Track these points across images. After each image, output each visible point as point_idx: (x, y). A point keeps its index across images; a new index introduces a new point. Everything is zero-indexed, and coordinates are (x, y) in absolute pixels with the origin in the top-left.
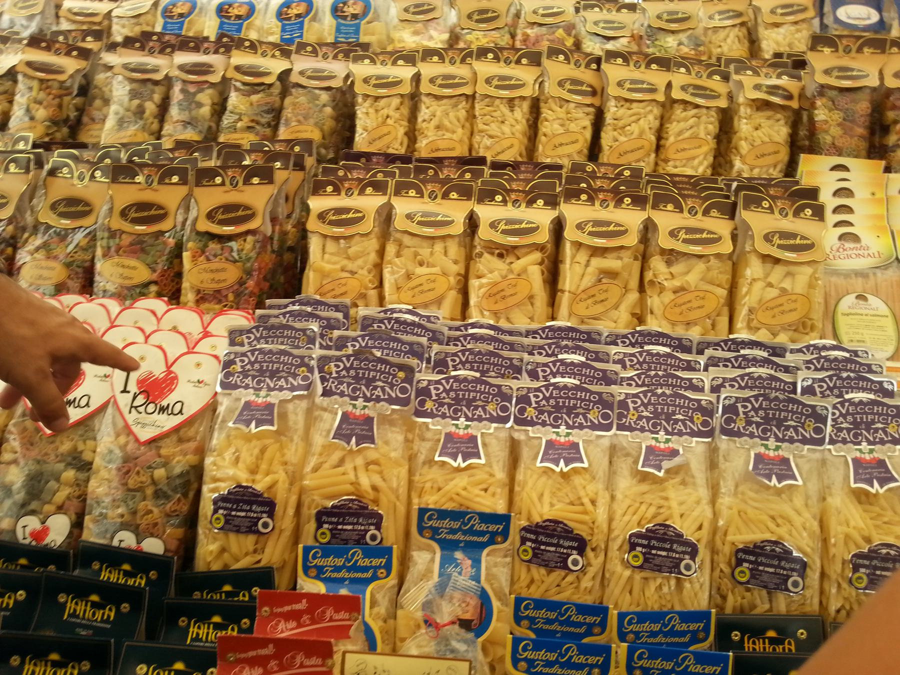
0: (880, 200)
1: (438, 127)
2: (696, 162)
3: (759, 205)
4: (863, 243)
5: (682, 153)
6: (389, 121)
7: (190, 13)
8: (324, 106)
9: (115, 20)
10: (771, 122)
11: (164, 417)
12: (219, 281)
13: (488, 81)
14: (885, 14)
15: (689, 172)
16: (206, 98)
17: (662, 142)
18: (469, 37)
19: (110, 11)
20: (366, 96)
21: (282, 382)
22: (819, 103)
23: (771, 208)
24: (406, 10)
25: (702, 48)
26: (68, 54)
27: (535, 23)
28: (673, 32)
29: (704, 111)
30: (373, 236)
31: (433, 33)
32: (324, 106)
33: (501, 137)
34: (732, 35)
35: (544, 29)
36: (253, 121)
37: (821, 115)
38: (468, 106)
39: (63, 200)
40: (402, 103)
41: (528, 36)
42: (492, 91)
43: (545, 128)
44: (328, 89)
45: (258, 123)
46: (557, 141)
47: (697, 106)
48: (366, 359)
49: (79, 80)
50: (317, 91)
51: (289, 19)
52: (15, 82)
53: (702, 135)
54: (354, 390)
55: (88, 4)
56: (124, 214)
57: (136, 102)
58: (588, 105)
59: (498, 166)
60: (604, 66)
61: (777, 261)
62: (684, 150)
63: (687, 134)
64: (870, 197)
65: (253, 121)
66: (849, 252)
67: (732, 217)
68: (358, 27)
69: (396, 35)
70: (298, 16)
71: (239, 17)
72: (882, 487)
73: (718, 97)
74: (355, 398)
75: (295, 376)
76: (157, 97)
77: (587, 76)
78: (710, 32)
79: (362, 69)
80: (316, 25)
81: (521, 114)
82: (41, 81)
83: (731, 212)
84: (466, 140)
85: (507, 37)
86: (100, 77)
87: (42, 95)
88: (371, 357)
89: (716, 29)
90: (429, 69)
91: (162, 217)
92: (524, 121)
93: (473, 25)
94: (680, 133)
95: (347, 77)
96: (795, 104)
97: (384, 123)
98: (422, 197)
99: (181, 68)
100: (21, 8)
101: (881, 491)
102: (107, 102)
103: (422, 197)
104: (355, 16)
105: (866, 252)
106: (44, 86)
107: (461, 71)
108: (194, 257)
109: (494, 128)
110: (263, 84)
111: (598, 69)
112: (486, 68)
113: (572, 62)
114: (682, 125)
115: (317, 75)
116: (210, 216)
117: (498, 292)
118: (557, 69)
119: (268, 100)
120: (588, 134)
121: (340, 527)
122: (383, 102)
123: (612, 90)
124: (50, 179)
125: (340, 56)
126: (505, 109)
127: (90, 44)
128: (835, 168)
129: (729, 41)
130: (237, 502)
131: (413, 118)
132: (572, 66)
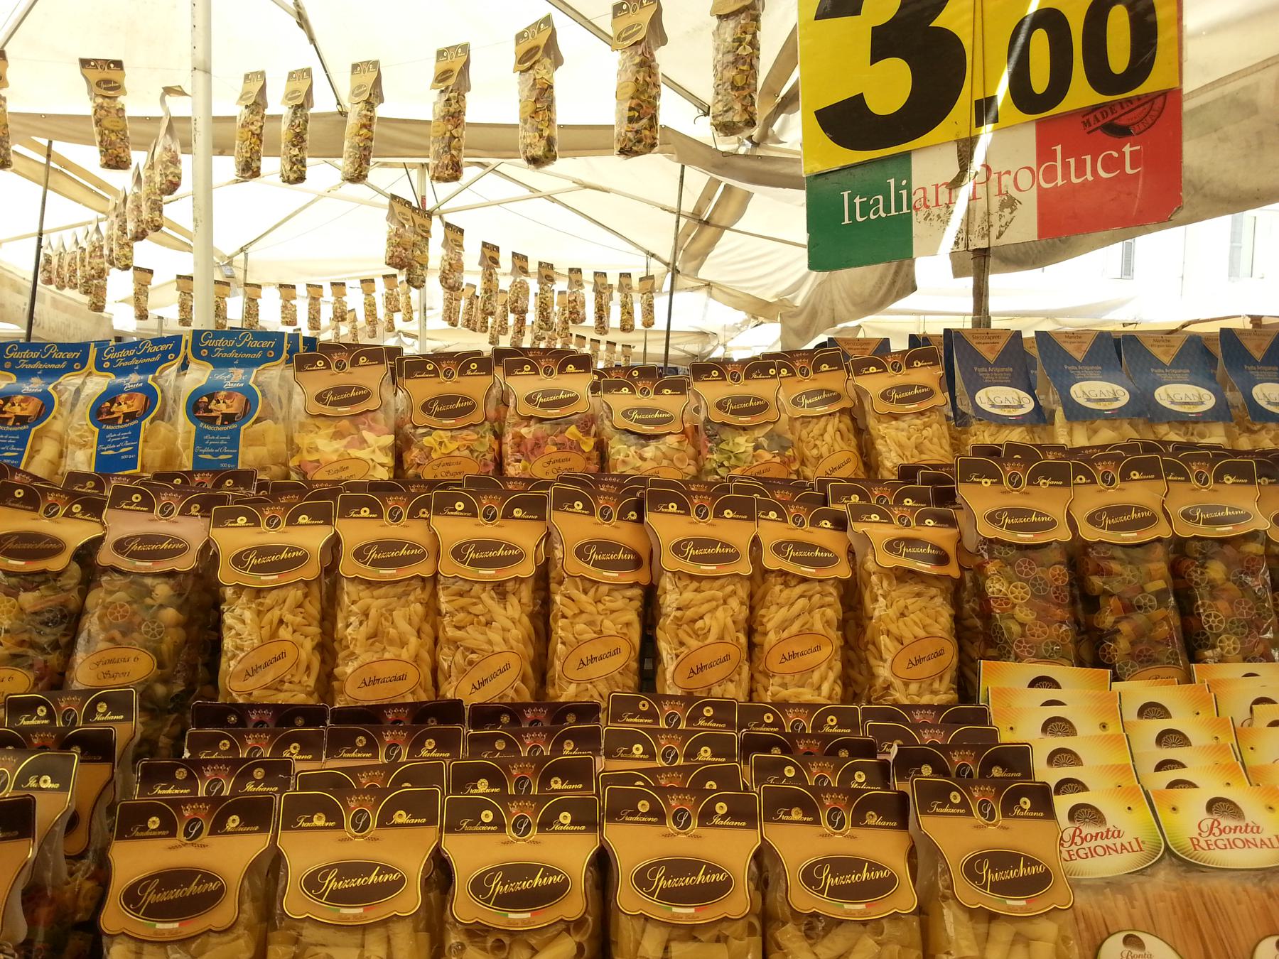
0: (1115, 739)
1: (374, 636)
2: (816, 676)
3: (946, 801)
4: (1110, 823)
5: (792, 662)
6: (284, 633)
8: (161, 606)
10: (921, 602)
13: (458, 553)
14: (1041, 398)
15: (808, 696)
17: (757, 639)
18: (427, 441)
20: (239, 589)
22: (991, 568)
23: (964, 804)
24: (320, 398)
25: (789, 453)
27: (531, 417)
28: (744, 429)
29: (817, 587)
30: (240, 930)
31: (367, 435)
32: (161, 606)
33: (488, 663)
34: (830, 428)
35: (546, 426)
36: (22, 643)
37: (995, 587)
38: (425, 596)
40: (306, 596)
41: (522, 437)
43: (561, 629)
44: (171, 574)
45: (33, 645)
46: (586, 652)
47: (804, 580)
50: (149, 581)
51: (114, 421)
53: (818, 626)
58: (631, 586)
59: (485, 715)
60: (650, 517)
61: (992, 917)
62: (793, 656)
63: (795, 628)
64: (1100, 732)
65: (22, 643)
66: (1093, 844)
67: (904, 825)
68: (235, 436)
69: (303, 440)
70: (130, 416)
71: (21, 420)
77: (621, 532)
78: (798, 424)
79: (235, 538)
80: (163, 427)
83: (898, 811)
84: (426, 657)
85: (489, 437)
89: (806, 420)
90: (358, 530)
92: (526, 620)
93: (432, 421)
94: (783, 627)
95: (207, 545)
96: (953, 570)
97: (274, 635)
98: (340, 826)
103: (340, 826)
104: (229, 418)
105: (1118, 842)
107: (411, 531)
109: (473, 636)
110: (44, 572)
111: (640, 520)
112: (454, 529)
113: (597, 512)
114: (783, 613)
115: (150, 547)
118: (575, 526)
119: (61, 597)
120: (635, 634)
122: (269, 600)
123: (669, 561)
125: (195, 509)
126: (488, 599)
128: (1037, 682)
129: (827, 437)
131: (328, 617)
132: (598, 518)
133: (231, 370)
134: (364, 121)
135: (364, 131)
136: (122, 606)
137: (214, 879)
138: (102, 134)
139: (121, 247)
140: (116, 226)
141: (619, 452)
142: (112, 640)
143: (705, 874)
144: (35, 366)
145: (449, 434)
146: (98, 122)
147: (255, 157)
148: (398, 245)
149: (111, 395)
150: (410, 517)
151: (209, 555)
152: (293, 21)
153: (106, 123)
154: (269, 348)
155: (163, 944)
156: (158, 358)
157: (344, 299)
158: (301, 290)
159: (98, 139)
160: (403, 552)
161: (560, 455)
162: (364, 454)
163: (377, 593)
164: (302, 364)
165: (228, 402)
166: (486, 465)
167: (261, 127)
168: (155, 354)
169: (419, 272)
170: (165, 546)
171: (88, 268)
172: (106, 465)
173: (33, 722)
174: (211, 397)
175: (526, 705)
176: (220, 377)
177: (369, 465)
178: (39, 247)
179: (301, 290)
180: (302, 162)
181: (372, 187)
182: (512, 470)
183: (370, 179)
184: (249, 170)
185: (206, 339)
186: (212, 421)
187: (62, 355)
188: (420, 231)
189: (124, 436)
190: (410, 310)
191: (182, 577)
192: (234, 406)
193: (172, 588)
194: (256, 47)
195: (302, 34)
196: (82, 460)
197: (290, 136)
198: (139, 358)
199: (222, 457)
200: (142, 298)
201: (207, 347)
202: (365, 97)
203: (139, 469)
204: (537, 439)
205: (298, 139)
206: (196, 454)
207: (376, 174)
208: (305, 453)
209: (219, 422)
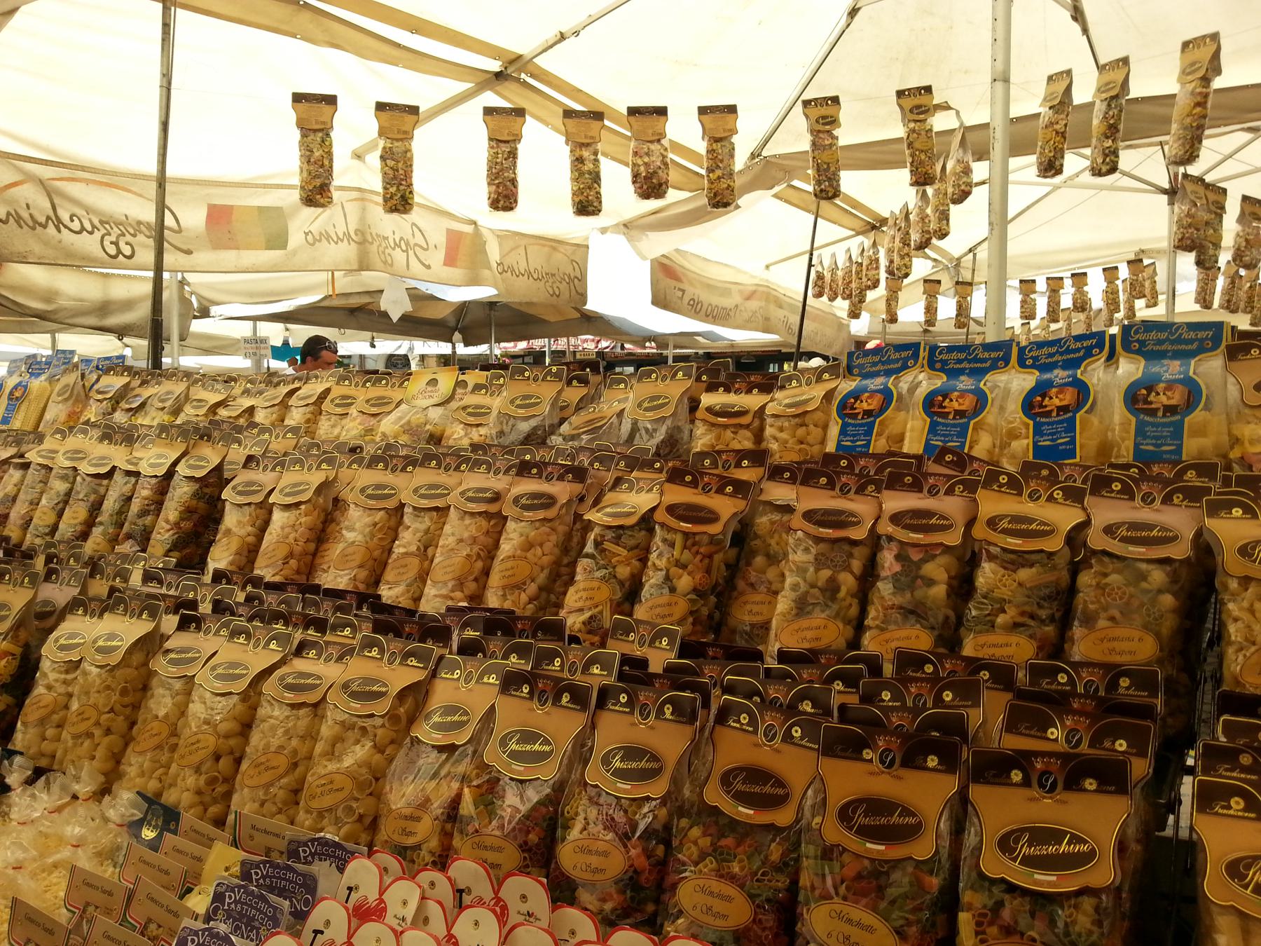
7: (882, 410)
9: (769, 421)
16: (938, 570)
19: (763, 408)
32: (1160, 591)
36: (1023, 614)
39: (740, 769)
45: (1032, 617)
49: (733, 526)
50: (1144, 566)
52: (651, 531)
56: (845, 815)
57: (826, 574)
71: (960, 414)
76: (857, 565)
82: (686, 535)
86: (763, 521)
87: (687, 555)
95: (1199, 534)
99: (896, 518)
100: (646, 409)
102: (774, 559)
106: (689, 543)
108: (979, 924)
115: (1139, 534)
119: (1050, 577)
124: (718, 728)
127: (747, 473)
133: (1165, 362)
134: (1199, 99)
135: (1198, 110)
136: (1119, 588)
138: (912, 155)
139: (902, 257)
140: (897, 240)
142: (1112, 619)
143: (1069, 843)
144: (877, 368)
146: (910, 145)
147: (1059, 155)
148: (1190, 226)
149: (1041, 389)
150: (1164, 502)
151: (1205, 549)
152: (1067, 15)
153: (917, 145)
154: (1206, 338)
156: (1081, 353)
157: (1086, 288)
158: (1041, 286)
159: (909, 160)
164: (1234, 353)
165: (1169, 393)
167: (1066, 125)
168: (1078, 350)
169: (1211, 252)
171: (864, 279)
172: (1144, 458)
173: (1053, 687)
174: (1150, 389)
176: (1155, 369)
178: (810, 265)
179: (1041, 286)
180: (1115, 153)
181: (1124, 174)
183: (1121, 165)
184: (1051, 167)
185: (1136, 332)
186: (1153, 412)
187: (986, 355)
188: (1213, 208)
190: (1155, 295)
191: (1177, 564)
192: (1176, 398)
193: (1167, 575)
194: (1049, 51)
195: (1076, 28)
196: (913, 445)
197: (1103, 128)
198: (1062, 354)
199: (1165, 448)
200: (893, 303)
201: (1138, 341)
202: (1201, 73)
203: (1078, 459)
205: (1112, 131)
206: (1136, 445)
207: (1127, 159)
208: (1247, 444)
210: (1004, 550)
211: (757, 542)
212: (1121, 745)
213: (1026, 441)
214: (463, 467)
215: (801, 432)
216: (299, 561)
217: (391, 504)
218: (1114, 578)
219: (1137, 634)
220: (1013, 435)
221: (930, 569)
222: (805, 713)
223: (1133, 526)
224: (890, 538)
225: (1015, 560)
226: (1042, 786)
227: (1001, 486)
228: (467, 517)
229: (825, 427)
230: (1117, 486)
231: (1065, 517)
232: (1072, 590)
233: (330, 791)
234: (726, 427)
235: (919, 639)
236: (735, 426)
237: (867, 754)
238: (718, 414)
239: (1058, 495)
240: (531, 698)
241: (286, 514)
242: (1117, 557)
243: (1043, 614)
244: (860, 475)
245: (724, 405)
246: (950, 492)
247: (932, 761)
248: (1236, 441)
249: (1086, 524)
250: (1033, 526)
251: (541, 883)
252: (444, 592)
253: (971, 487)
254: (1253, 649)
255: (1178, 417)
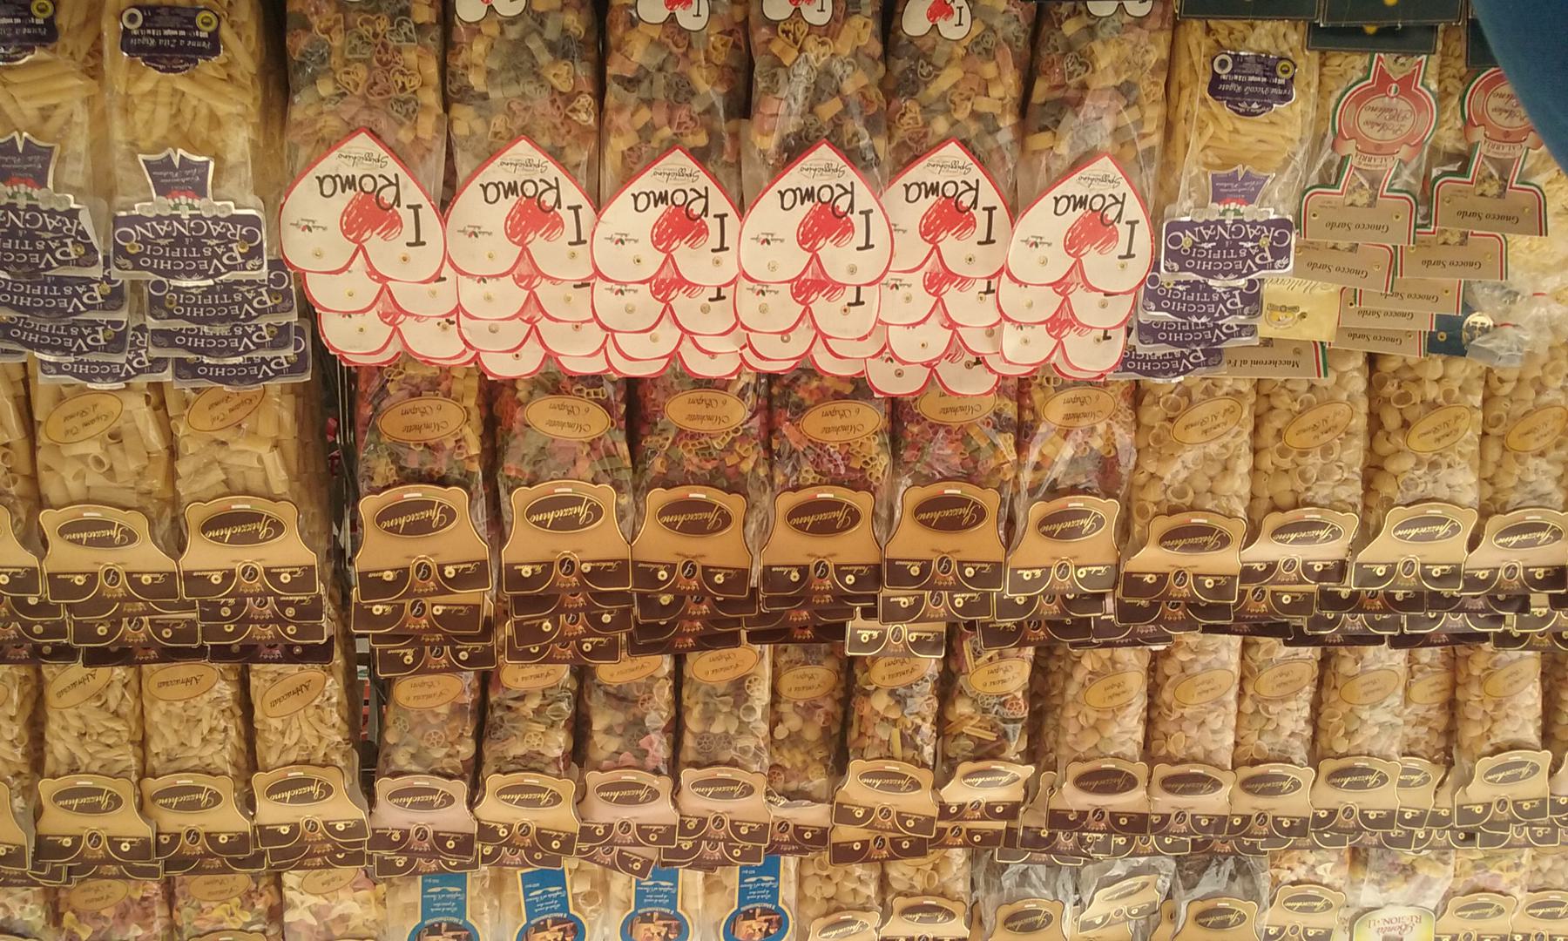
11: (507, 178)
12: (700, 401)
16: (604, 744)
21: (162, 229)
26: (1083, 815)
39: (713, 531)
42: (106, 784)
44: (395, 775)
45: (509, 708)
48: (18, 266)
50: (414, 768)
54: (34, 220)
55: (929, 930)
68: (426, 914)
72: (169, 156)
73: (59, 797)
74: (30, 208)
75: (144, 240)
76: (689, 741)
81: (60, 746)
88: (12, 269)
91: (795, 512)
101: (170, 150)
113: (1270, 819)
115: (421, 799)
116: (725, 520)
117: (237, 407)
121: (18, 21)
123: (125, 789)
130: (179, 49)
137: (921, 521)
141: (32, 912)
142: (437, 715)
145: (224, 925)
155: (246, 492)
160: (616, 795)
161: (96, 906)
162: (312, 900)
163: (196, 762)
166: (183, 893)
170: (1501, 776)
175: (693, 649)
177: (302, 888)
182: (153, 887)
189: (437, 907)
204: (123, 923)
206: (464, 891)
209: (444, 926)
210: (541, 772)
211: (818, 756)
212: (378, 610)
213: (576, 890)
214: (1237, 822)
215: (830, 891)
216: (1469, 675)
217: (1328, 766)
218: (439, 753)
219: (412, 703)
220: (589, 897)
221: (613, 744)
222: (665, 592)
223: (428, 806)
224: (657, 772)
225: (530, 762)
226: (427, 567)
227: (557, 837)
228: (1201, 756)
229: (801, 898)
230: (450, 844)
231: (493, 810)
232: (480, 737)
233: (1203, 422)
234: (924, 893)
235: (609, 673)
236: (913, 895)
237: (587, 568)
238: (938, 909)
239: (503, 832)
240: (960, 563)
241: (1511, 736)
242: (439, 774)
243: (498, 713)
244: (612, 843)
245: (933, 920)
246: (609, 828)
247: (526, 571)
248: (382, 902)
249: (938, 786)
250: (517, 798)
251: (879, 392)
252: (1204, 659)
253: (587, 834)
254: (316, 702)
255: (427, 922)
